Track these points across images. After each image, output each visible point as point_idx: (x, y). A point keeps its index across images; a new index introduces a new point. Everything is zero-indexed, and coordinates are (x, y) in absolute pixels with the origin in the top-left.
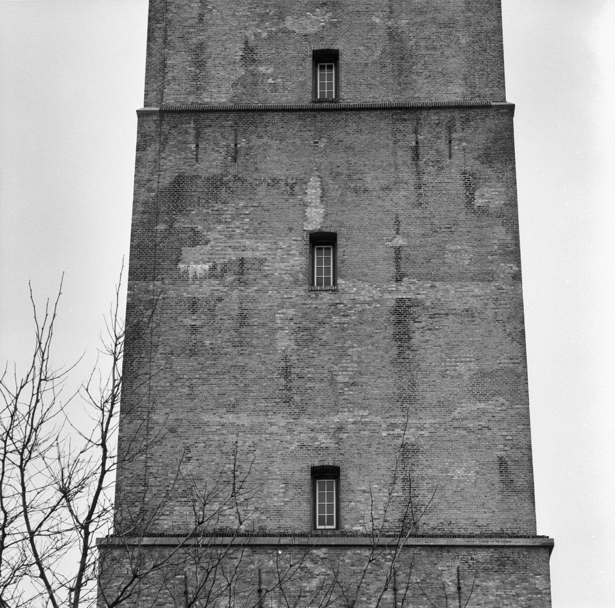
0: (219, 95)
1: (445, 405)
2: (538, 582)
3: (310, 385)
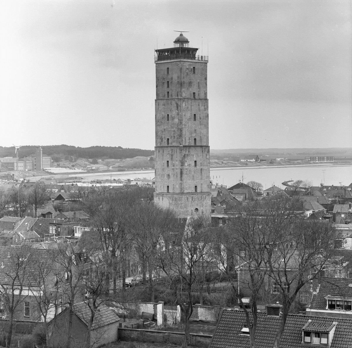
0: (187, 144)
1: (204, 179)
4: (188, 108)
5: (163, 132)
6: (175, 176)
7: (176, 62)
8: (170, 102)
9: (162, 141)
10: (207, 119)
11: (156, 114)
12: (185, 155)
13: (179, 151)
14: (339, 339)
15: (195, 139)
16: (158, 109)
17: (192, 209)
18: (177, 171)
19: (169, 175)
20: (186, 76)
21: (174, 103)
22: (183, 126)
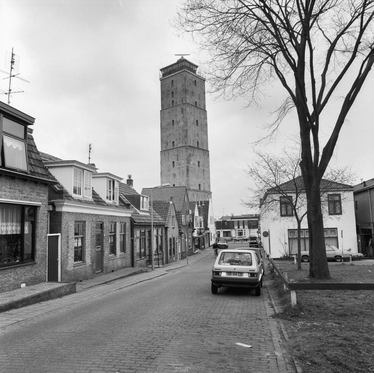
0: (192, 145)
1: (206, 180)
4: (191, 113)
5: (168, 137)
6: (181, 174)
7: (180, 73)
8: (175, 109)
9: (167, 145)
15: (198, 142)
16: (163, 118)
18: (183, 169)
19: (175, 175)
20: (190, 85)
21: (179, 109)
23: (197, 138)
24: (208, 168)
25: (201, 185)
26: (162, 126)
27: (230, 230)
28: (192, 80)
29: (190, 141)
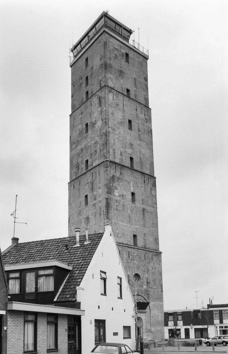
0: (117, 161)
2: (160, 258)
3: (133, 220)
6: (98, 215)
10: (150, 136)
11: (70, 134)
12: (113, 176)
13: (103, 169)
14: (65, 346)
17: (129, 273)
19: (88, 218)
21: (95, 100)
22: (110, 130)
23: (129, 151)
24: (153, 207)
25: (138, 237)
26: (72, 139)
27: (205, 327)
28: (121, 51)
29: (114, 153)
